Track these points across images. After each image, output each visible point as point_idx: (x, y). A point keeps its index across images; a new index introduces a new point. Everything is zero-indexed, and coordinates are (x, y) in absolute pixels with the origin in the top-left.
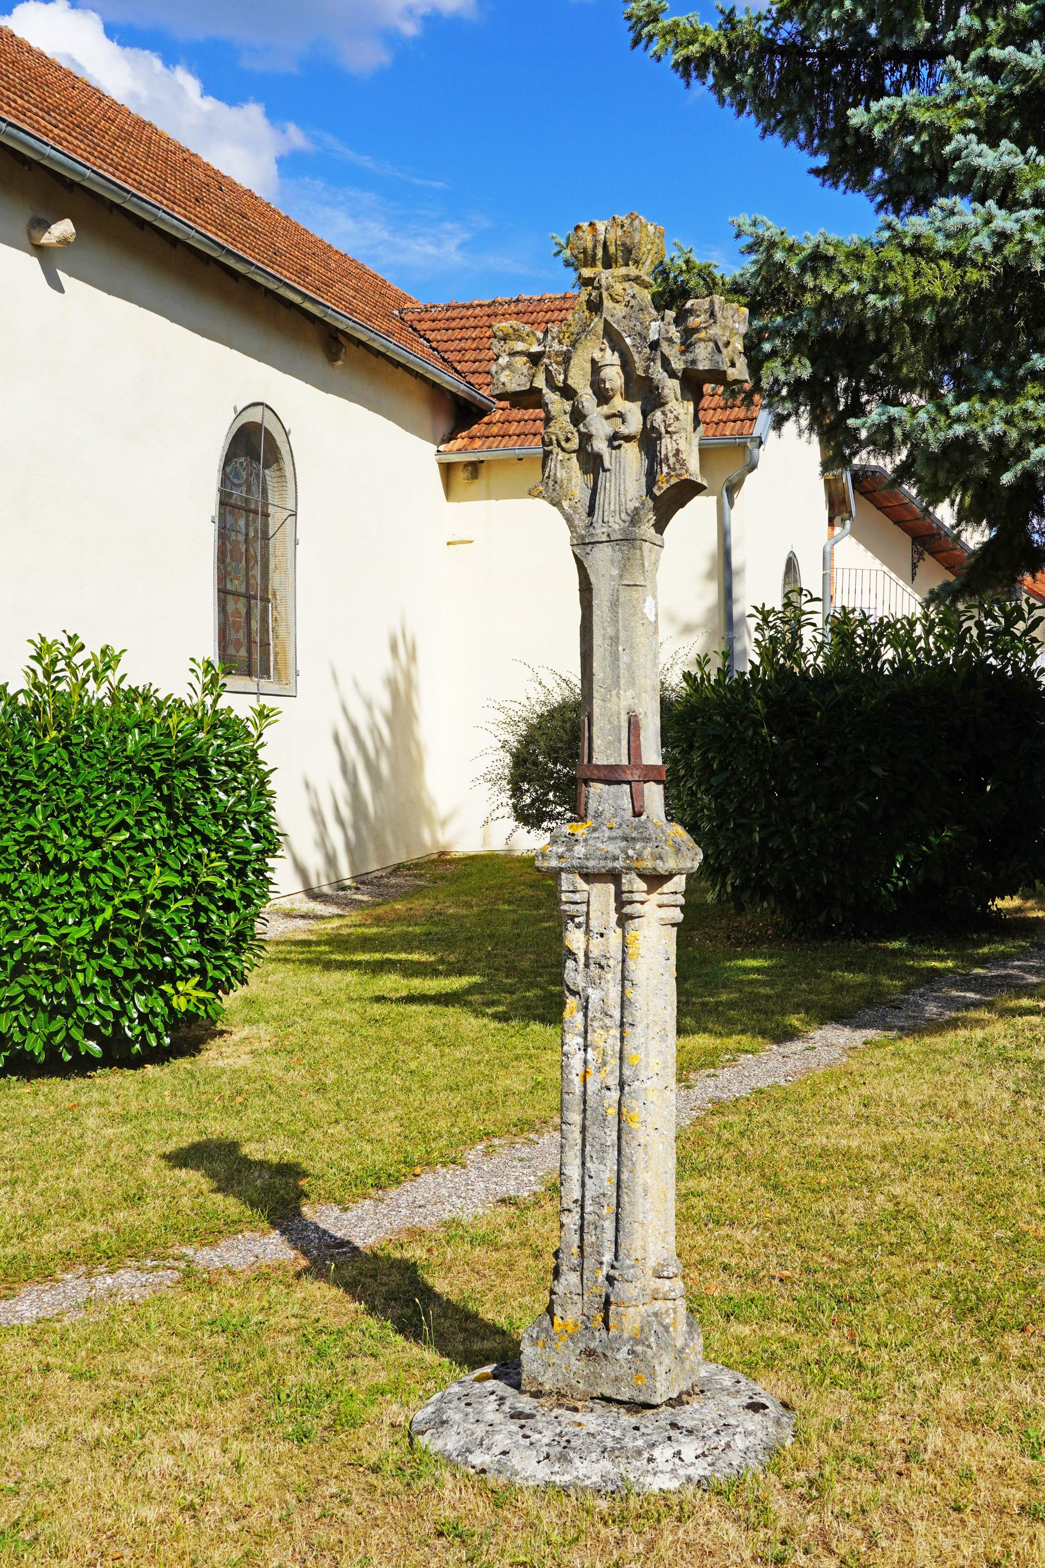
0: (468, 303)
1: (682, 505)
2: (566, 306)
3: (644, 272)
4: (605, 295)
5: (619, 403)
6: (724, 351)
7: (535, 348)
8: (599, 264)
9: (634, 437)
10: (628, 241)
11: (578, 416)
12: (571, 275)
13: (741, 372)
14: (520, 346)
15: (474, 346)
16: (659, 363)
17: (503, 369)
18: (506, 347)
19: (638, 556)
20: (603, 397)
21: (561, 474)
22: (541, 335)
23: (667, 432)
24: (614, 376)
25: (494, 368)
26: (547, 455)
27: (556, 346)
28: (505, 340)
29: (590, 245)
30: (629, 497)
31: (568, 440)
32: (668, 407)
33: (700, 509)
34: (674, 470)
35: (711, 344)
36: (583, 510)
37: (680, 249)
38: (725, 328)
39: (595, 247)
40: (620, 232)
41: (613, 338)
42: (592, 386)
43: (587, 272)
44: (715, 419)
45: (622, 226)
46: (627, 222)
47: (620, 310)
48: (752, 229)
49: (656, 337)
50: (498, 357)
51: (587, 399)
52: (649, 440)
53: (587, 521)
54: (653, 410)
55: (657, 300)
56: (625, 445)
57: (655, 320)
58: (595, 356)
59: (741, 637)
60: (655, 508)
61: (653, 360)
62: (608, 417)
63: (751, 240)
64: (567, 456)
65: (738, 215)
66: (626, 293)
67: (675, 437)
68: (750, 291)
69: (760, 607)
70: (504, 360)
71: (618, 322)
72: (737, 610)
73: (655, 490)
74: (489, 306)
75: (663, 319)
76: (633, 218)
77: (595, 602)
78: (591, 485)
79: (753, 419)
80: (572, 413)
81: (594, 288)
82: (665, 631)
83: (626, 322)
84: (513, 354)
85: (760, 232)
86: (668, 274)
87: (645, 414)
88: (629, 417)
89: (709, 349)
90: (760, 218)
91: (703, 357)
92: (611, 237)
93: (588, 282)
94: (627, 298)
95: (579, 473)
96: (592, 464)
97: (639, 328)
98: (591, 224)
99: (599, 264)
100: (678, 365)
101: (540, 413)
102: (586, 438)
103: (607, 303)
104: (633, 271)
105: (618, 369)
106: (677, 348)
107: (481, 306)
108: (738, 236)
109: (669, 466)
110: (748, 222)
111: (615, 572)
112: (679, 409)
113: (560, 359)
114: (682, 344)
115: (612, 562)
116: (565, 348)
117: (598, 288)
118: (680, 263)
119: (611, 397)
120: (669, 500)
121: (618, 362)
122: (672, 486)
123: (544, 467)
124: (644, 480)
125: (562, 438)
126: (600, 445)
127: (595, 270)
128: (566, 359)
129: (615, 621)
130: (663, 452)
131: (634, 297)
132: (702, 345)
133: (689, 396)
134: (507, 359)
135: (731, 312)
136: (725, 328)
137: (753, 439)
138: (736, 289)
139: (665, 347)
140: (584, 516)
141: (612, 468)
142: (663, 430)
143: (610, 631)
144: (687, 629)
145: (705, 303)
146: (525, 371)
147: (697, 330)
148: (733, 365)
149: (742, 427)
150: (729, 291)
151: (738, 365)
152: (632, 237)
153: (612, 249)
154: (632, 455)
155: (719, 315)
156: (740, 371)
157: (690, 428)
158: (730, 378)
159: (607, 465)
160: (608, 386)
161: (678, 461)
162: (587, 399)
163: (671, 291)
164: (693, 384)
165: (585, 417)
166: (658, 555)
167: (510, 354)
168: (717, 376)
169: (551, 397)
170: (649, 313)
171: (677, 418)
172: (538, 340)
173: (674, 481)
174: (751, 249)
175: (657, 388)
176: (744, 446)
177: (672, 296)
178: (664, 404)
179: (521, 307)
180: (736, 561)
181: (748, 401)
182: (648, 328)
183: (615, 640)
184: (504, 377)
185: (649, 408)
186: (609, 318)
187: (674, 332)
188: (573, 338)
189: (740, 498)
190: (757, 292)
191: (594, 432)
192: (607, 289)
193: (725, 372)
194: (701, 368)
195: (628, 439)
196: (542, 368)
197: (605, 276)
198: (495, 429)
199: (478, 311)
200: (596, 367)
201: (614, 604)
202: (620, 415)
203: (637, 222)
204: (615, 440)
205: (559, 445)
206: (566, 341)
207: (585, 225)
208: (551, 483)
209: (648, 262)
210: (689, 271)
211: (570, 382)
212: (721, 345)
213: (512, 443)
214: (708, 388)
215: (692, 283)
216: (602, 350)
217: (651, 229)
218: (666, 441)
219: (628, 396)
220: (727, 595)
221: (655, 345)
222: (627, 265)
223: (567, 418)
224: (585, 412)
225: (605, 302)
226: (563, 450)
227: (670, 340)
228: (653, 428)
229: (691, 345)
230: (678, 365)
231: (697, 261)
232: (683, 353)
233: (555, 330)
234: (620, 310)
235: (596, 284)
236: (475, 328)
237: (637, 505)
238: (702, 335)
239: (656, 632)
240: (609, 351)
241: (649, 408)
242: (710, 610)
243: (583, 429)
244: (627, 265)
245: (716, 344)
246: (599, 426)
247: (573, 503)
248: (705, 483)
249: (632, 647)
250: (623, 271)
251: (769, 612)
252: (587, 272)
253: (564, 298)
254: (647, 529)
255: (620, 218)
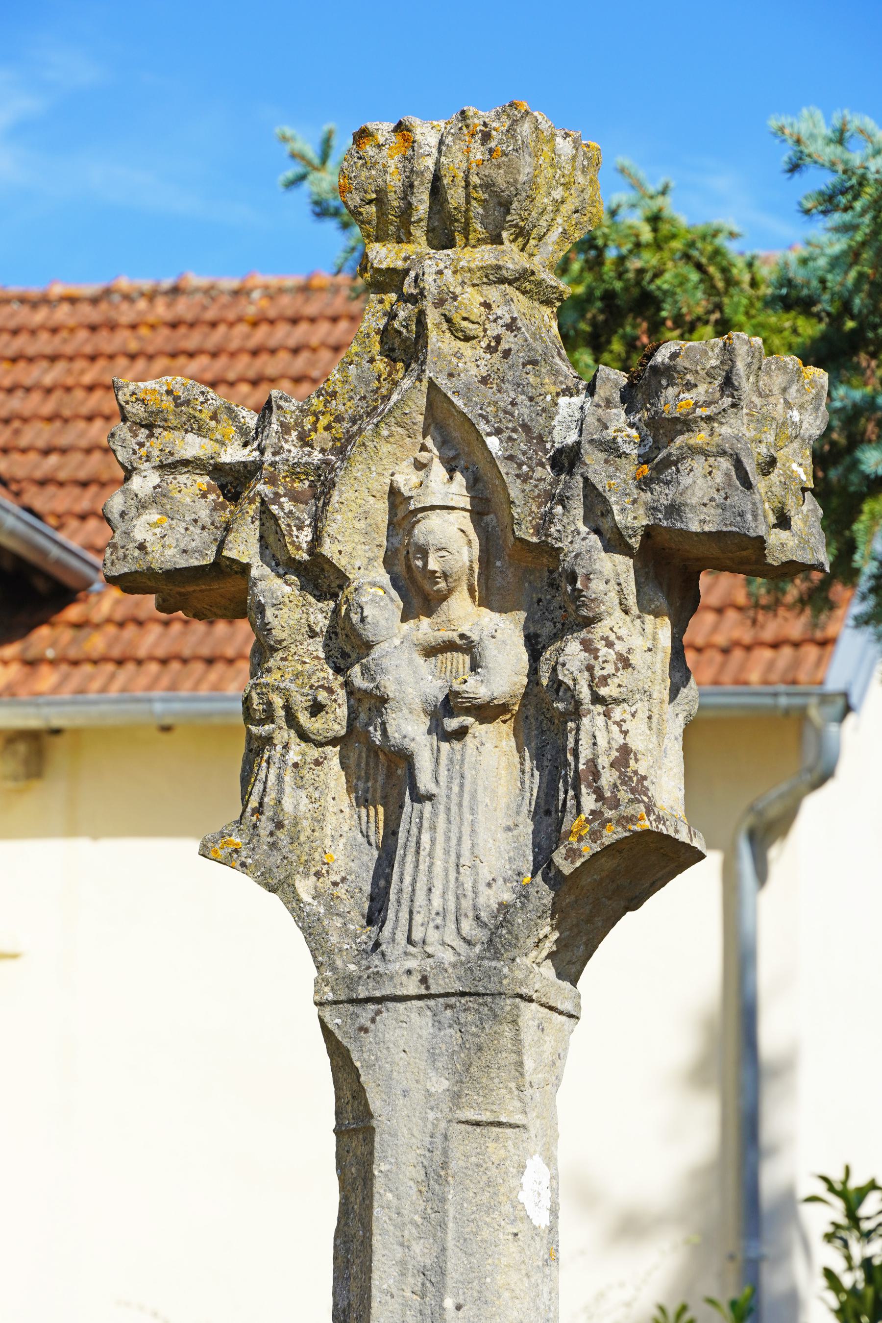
0: (34, 290)
1: (635, 903)
2: (311, 309)
3: (541, 260)
4: (433, 317)
5: (464, 614)
6: (760, 484)
7: (234, 454)
8: (419, 233)
9: (504, 708)
10: (500, 179)
11: (347, 645)
12: (332, 243)
13: (804, 543)
14: (192, 446)
15: (48, 408)
16: (578, 511)
17: (142, 506)
18: (154, 447)
19: (506, 1042)
20: (419, 592)
21: (294, 802)
22: (251, 420)
23: (597, 699)
24: (451, 538)
25: (116, 502)
26: (257, 749)
27: (293, 450)
28: (150, 427)
29: (394, 181)
30: (485, 874)
31: (316, 709)
32: (601, 629)
33: (687, 904)
34: (615, 804)
35: (725, 464)
36: (353, 908)
37: (636, 185)
38: (762, 420)
39: (410, 186)
40: (478, 153)
41: (451, 435)
42: (388, 563)
43: (385, 255)
44: (721, 639)
45: (486, 137)
46: (499, 126)
47: (472, 361)
48: (831, 152)
49: (572, 438)
50: (129, 472)
51: (376, 601)
52: (545, 720)
53: (366, 935)
54: (557, 636)
55: (571, 316)
56: (479, 730)
57: (568, 392)
58: (400, 481)
59: (783, 1256)
60: (556, 909)
61: (563, 501)
62: (431, 651)
63: (827, 181)
64: (314, 753)
65: (794, 112)
66: (489, 314)
67: (618, 713)
68: (825, 305)
69: (837, 1176)
70: (144, 483)
71: (466, 393)
72: (772, 1178)
73: (558, 857)
74: (95, 301)
75: (591, 390)
76: (513, 113)
77: (380, 1167)
78: (377, 837)
79: (826, 643)
80: (332, 633)
81: (405, 298)
82: (576, 1234)
83: (490, 392)
84: (171, 466)
85: (856, 159)
86: (601, 252)
87: (535, 646)
88: (491, 653)
89: (719, 477)
90: (856, 121)
91: (700, 496)
92: (455, 163)
93: (388, 280)
94: (494, 330)
95: (345, 801)
96: (384, 778)
97: (524, 410)
98: (400, 128)
99: (419, 233)
100: (630, 516)
101: (238, 636)
102: (369, 705)
103: (439, 341)
104: (512, 257)
105: (464, 520)
106: (629, 469)
107: (72, 300)
108: (794, 167)
109: (599, 794)
110: (825, 131)
111: (440, 1085)
112: (632, 636)
113: (302, 486)
114: (645, 459)
115: (433, 1056)
116: (317, 456)
117: (413, 299)
118: (635, 220)
119: (444, 597)
120: (599, 883)
121: (465, 502)
122: (607, 849)
123: (247, 779)
124: (527, 828)
125: (300, 702)
126: (408, 728)
127: (408, 249)
128: (321, 486)
129: (435, 1224)
130: (585, 753)
131: (512, 326)
132: (699, 464)
133: (661, 601)
134: (154, 478)
135: (779, 380)
136: (762, 420)
137: (825, 699)
138: (792, 299)
139: (593, 458)
140: (356, 922)
141: (440, 792)
142: (585, 694)
143: (421, 1252)
144: (631, 1228)
145: (705, 348)
146: (204, 514)
147: (684, 424)
148: (783, 522)
149: (796, 664)
150: (770, 303)
151: (797, 522)
152: (512, 169)
153: (455, 197)
154: (495, 761)
155: (746, 385)
156: (803, 539)
157: (661, 690)
158: (775, 558)
159: (425, 782)
160: (433, 564)
161: (625, 779)
162: (376, 601)
163: (609, 296)
164: (671, 570)
165: (369, 646)
166: (563, 1041)
167: (161, 467)
168: (741, 553)
169: (273, 588)
170: (555, 372)
171: (625, 662)
172: (243, 431)
173: (611, 835)
174: (829, 202)
175: (572, 577)
176: (800, 716)
177: (617, 312)
178: (588, 622)
179: (183, 308)
180: (772, 1036)
181: (819, 600)
182: (549, 412)
183: (433, 1278)
184: (143, 529)
185: (547, 629)
186: (442, 381)
187: (620, 424)
188: (340, 429)
189: (781, 856)
190: (846, 308)
191: (390, 688)
192: (440, 303)
193: (760, 541)
194: (695, 527)
195: (487, 712)
196: (252, 509)
197: (436, 268)
198: (97, 643)
199: (63, 313)
200: (402, 513)
201: (436, 1175)
202: (466, 646)
203: (526, 128)
204: (450, 714)
205: (291, 720)
206: (321, 437)
207: (383, 129)
208: (265, 826)
209: (554, 235)
210: (658, 245)
211: (328, 549)
212: (750, 466)
213: (143, 680)
214: (715, 586)
215: (665, 282)
216: (420, 466)
217: (564, 146)
218: (593, 722)
219: (489, 596)
220: (746, 1136)
221: (566, 460)
222: (497, 240)
223: (317, 647)
224: (369, 633)
225: (433, 336)
226: (304, 736)
227: (611, 448)
228: (557, 685)
229: (667, 463)
230: (630, 516)
231: (684, 215)
232: (644, 484)
233: (292, 406)
234: (472, 361)
235: (408, 288)
236: (53, 359)
237: (507, 897)
238: (700, 438)
239: (552, 1258)
240: (438, 471)
241: (547, 629)
242: (697, 1175)
243: (360, 682)
244: (497, 240)
245: (739, 465)
246: (405, 673)
247: (325, 883)
248: (698, 843)
249: (481, 1300)
250: (483, 255)
251: (862, 1193)
252: (385, 255)
253: (306, 289)
254: (536, 970)
255: (480, 116)
